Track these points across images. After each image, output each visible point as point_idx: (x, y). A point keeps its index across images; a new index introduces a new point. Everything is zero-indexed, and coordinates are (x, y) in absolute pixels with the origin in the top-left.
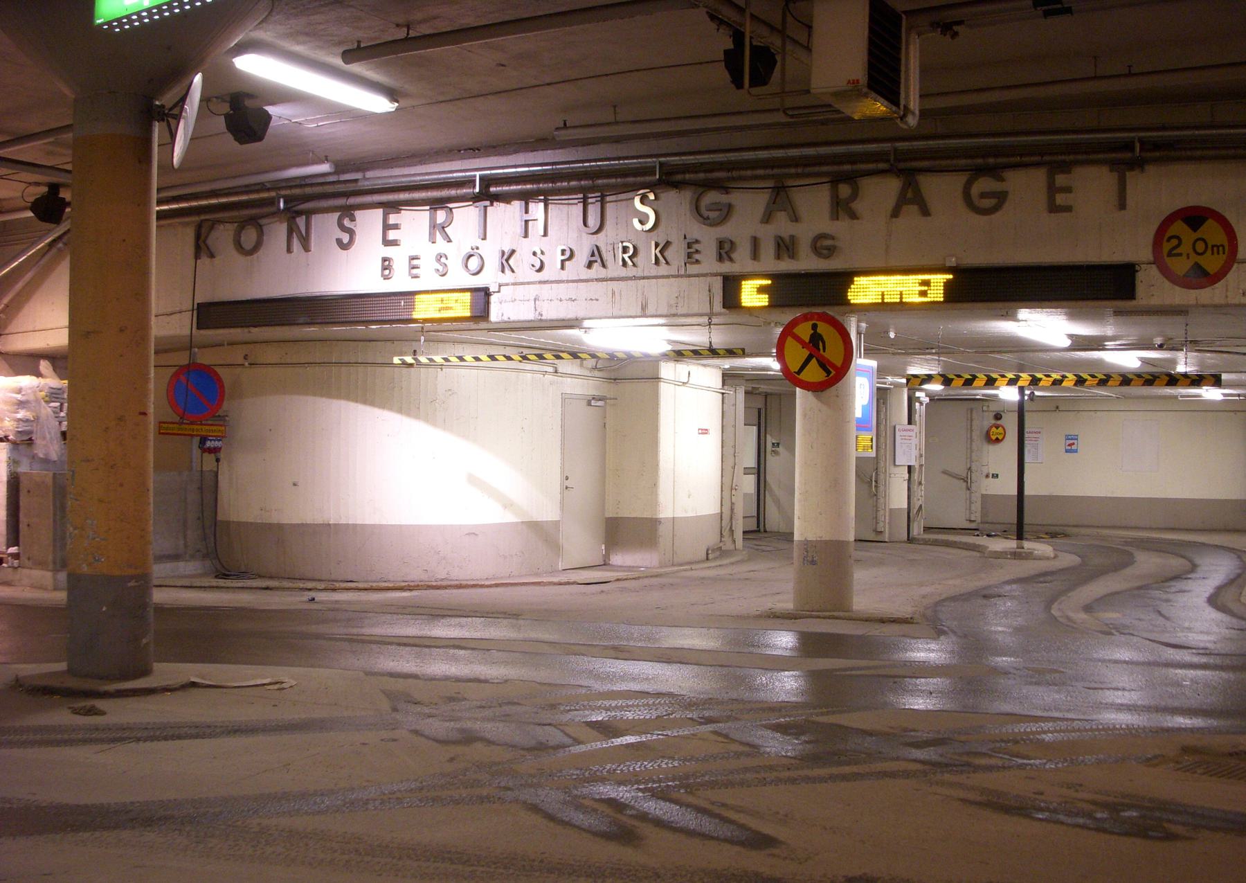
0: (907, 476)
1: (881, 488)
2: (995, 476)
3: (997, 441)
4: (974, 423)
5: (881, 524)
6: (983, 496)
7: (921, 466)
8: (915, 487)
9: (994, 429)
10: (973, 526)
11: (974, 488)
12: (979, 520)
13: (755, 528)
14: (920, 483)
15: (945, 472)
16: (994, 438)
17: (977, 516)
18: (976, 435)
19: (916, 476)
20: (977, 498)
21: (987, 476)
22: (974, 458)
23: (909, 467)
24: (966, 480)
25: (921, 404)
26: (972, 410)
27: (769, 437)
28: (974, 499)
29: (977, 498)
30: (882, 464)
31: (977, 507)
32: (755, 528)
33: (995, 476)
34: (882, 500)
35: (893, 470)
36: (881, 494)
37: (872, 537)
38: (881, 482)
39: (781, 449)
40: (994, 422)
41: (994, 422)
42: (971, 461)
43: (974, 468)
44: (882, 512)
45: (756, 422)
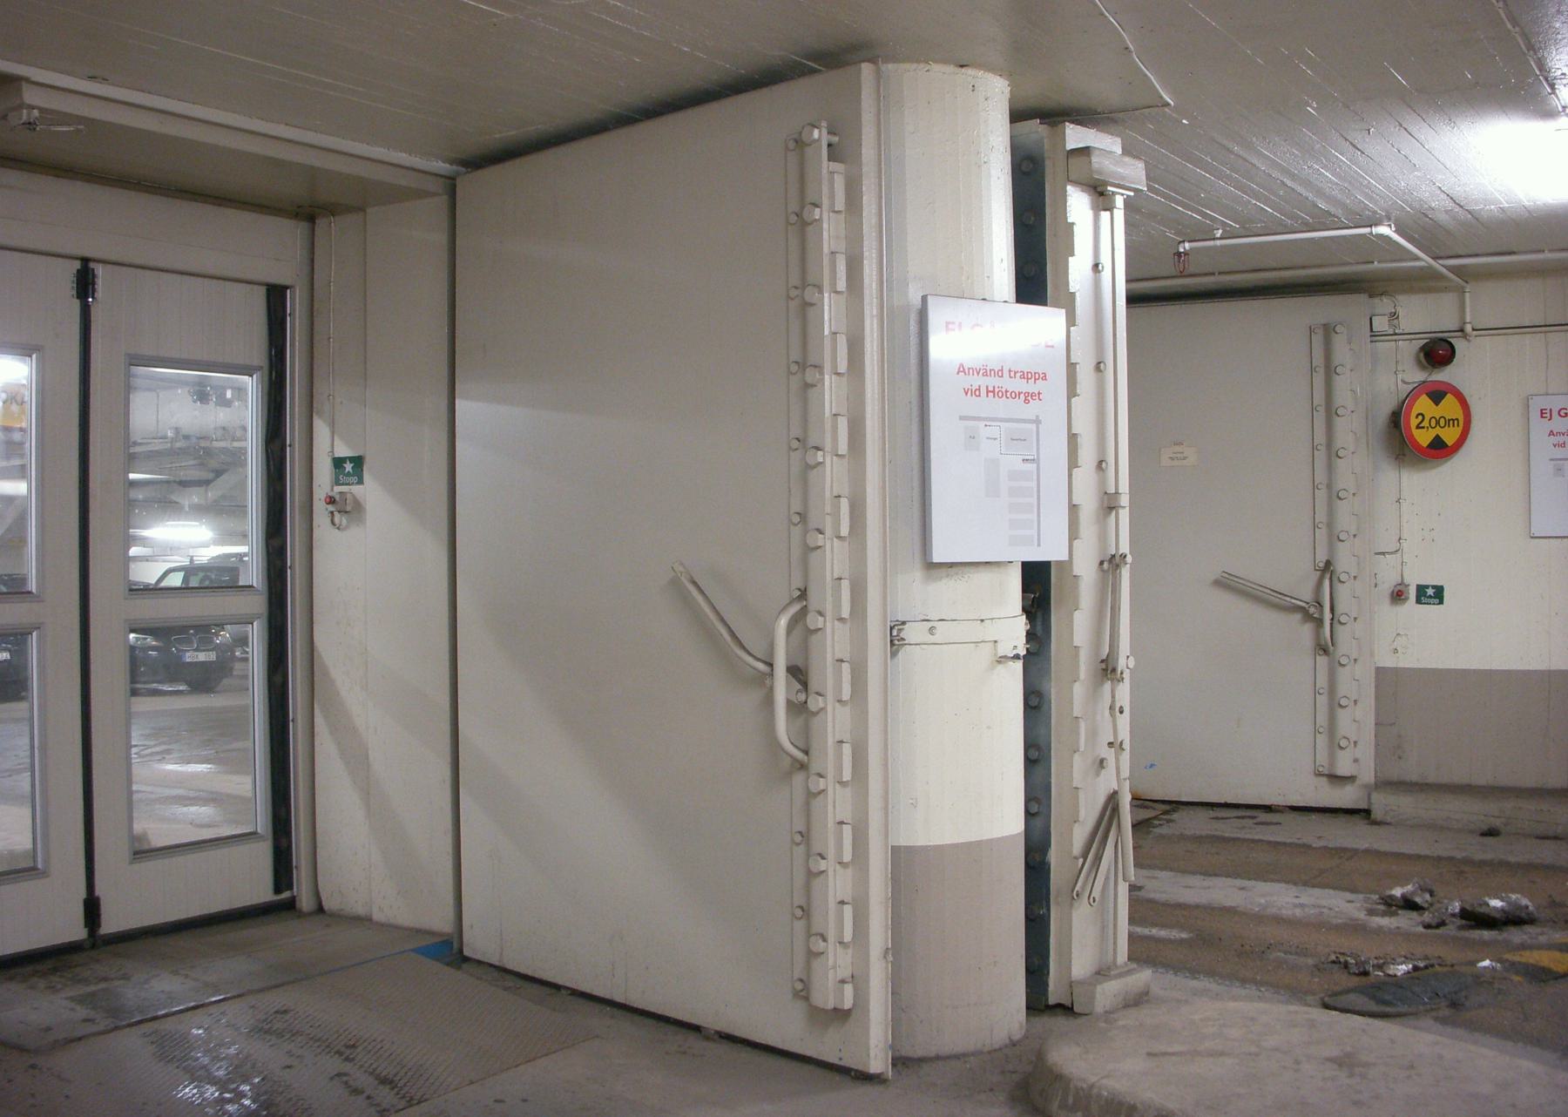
0: (1014, 631)
1: (835, 722)
2: (1432, 595)
3: (1440, 450)
4: (1342, 383)
5: (837, 962)
6: (1380, 672)
7: (1111, 564)
8: (1073, 693)
9: (1424, 404)
10: (1345, 797)
11: (1346, 644)
12: (1367, 775)
13: (261, 890)
14: (1107, 669)
15: (1225, 583)
16: (1424, 438)
17: (1359, 760)
18: (1349, 431)
19: (1077, 626)
20: (1357, 683)
21: (1398, 596)
22: (1345, 521)
23: (1037, 578)
24: (1317, 615)
25: (1100, 195)
26: (1328, 330)
27: (321, 429)
28: (1345, 687)
29: (1357, 683)
30: (834, 559)
31: (1358, 721)
32: (261, 890)
33: (1432, 595)
34: (838, 804)
35: (918, 596)
36: (834, 760)
37: (788, 1030)
38: (831, 679)
39: (369, 491)
40: (1419, 376)
41: (1419, 376)
42: (1334, 538)
43: (1344, 564)
44: (838, 883)
45: (257, 351)
